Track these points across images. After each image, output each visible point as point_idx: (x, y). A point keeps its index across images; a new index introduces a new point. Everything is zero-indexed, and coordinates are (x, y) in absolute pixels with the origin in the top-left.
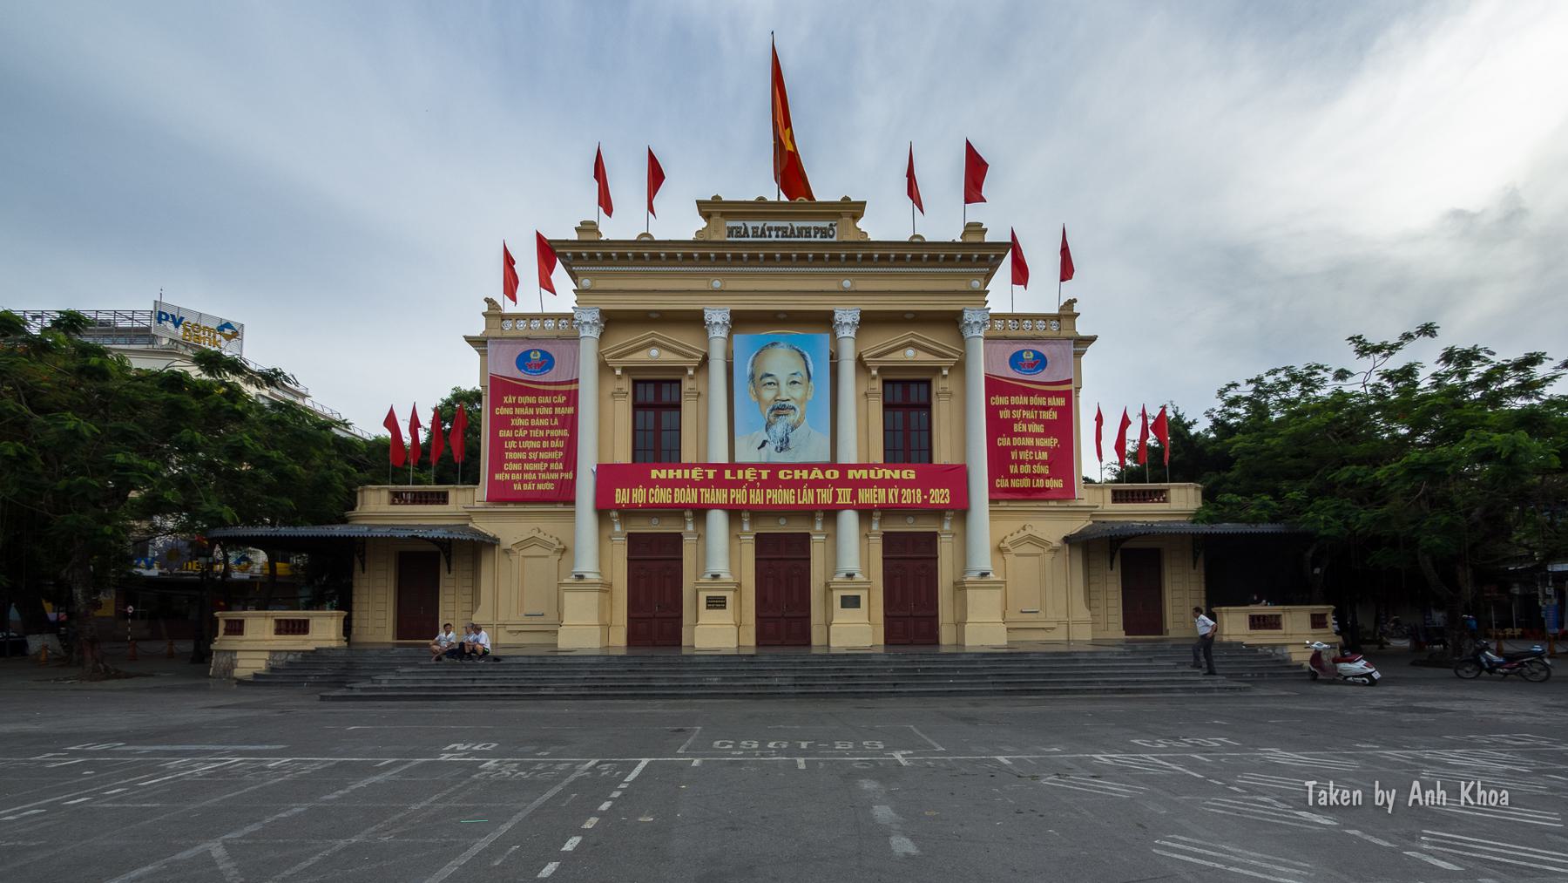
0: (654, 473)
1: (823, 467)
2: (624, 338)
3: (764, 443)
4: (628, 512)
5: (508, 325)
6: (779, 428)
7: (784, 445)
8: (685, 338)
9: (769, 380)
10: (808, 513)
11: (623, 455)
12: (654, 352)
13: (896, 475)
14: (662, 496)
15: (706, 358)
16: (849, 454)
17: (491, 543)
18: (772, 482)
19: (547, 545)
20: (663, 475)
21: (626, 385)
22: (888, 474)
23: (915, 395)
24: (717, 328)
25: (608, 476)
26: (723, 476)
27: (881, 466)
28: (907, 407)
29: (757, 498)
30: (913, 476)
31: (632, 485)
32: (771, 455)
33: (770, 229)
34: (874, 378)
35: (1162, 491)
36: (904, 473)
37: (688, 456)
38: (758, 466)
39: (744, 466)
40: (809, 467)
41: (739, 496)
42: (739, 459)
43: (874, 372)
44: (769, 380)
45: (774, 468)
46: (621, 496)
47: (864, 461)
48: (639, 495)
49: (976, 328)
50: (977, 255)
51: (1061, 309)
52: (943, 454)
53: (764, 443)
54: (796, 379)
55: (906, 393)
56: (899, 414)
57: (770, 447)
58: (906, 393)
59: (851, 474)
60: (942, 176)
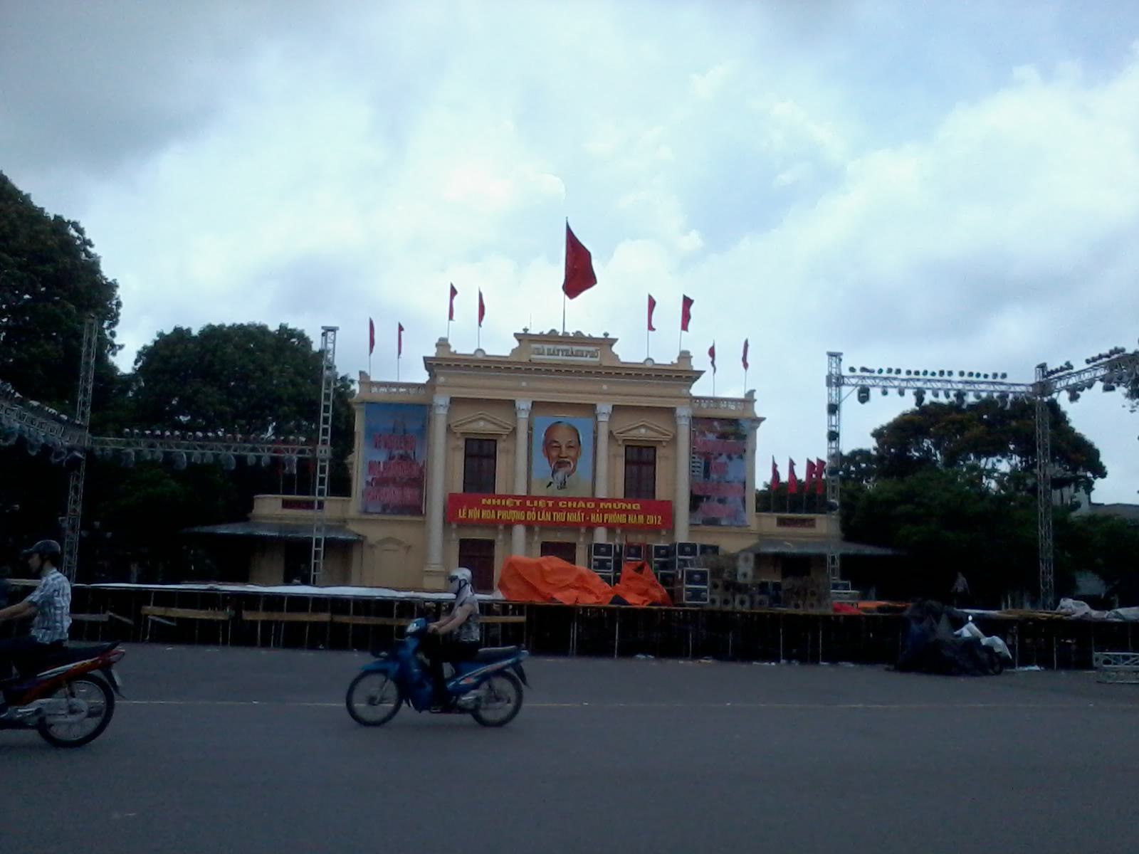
0: (484, 501)
1: (586, 500)
2: (463, 415)
3: (550, 483)
4: (464, 524)
5: (375, 390)
6: (560, 475)
7: (563, 485)
8: (502, 417)
9: (555, 444)
10: (492, 525)
11: (458, 488)
12: (482, 423)
13: (629, 507)
14: (486, 514)
15: (515, 430)
16: (601, 493)
17: (359, 542)
18: (556, 508)
19: (399, 543)
20: (489, 502)
21: (462, 443)
22: (624, 505)
23: (646, 455)
24: (523, 413)
25: (453, 503)
26: (524, 503)
27: (621, 501)
28: (640, 463)
29: (547, 517)
30: (639, 508)
31: (470, 507)
32: (554, 491)
33: (558, 350)
34: (619, 445)
35: (812, 520)
36: (634, 506)
37: (500, 488)
38: (546, 498)
39: (538, 498)
40: (577, 500)
41: (531, 516)
42: (534, 493)
43: (620, 442)
44: (555, 444)
45: (556, 500)
46: (462, 514)
47: (611, 496)
48: (474, 514)
49: (683, 419)
50: (683, 374)
51: (746, 395)
52: (661, 494)
53: (550, 483)
54: (572, 444)
55: (640, 452)
56: (635, 468)
57: (554, 486)
58: (640, 452)
59: (602, 505)
60: (669, 311)
